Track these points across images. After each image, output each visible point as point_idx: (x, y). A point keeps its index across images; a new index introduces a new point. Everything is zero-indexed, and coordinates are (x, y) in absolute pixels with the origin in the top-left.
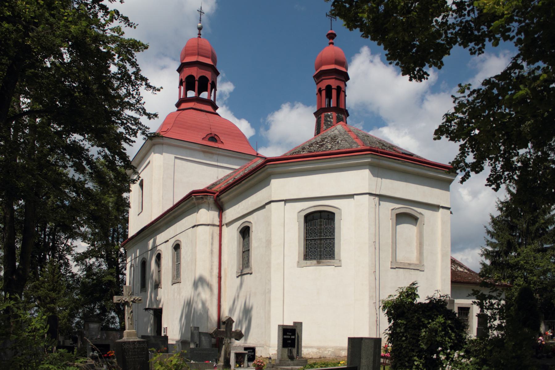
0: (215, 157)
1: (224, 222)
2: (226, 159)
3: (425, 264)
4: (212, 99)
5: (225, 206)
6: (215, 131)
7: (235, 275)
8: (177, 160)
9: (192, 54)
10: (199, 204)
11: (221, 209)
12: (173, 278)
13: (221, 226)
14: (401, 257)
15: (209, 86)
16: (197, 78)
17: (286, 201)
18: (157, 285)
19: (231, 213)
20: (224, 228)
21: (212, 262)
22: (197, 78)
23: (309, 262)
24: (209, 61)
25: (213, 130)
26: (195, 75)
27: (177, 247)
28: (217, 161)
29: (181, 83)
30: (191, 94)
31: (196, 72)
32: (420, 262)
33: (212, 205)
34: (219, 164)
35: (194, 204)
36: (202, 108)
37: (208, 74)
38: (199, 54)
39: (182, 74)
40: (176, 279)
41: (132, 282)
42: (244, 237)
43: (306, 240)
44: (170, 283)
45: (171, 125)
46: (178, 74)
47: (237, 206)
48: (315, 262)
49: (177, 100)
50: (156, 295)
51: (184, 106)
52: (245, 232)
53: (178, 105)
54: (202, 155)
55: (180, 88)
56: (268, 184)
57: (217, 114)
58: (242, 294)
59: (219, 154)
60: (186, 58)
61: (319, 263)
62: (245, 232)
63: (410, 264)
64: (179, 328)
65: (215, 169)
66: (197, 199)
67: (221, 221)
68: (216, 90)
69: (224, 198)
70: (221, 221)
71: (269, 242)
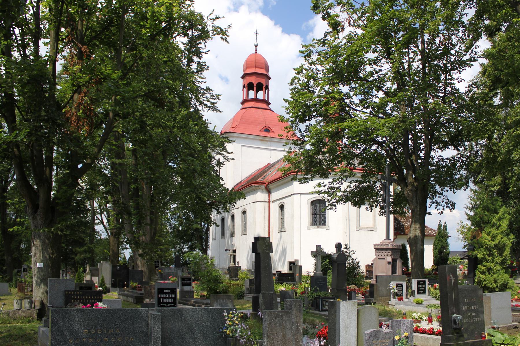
0: (269, 143)
1: (271, 200)
2: (277, 144)
3: (377, 227)
4: (266, 99)
5: (272, 191)
6: (268, 125)
7: (277, 232)
8: (243, 148)
9: (251, 67)
10: (256, 189)
11: (269, 192)
12: (242, 232)
13: (269, 202)
14: (363, 224)
15: (264, 89)
16: (255, 85)
17: (301, 194)
18: (232, 234)
19: (275, 195)
20: (271, 203)
21: (265, 223)
22: (255, 85)
23: (313, 227)
24: (263, 71)
25: (267, 123)
26: (253, 82)
27: (244, 213)
28: (270, 146)
29: (244, 87)
30: (252, 94)
31: (254, 80)
32: (374, 226)
33: (264, 190)
34: (271, 148)
35: (254, 189)
36: (259, 106)
37: (263, 81)
38: (256, 67)
39: (245, 81)
40: (244, 232)
41: (214, 231)
42: (282, 211)
43: (312, 215)
44: (240, 234)
45: (238, 122)
46: (242, 80)
47: (277, 192)
48: (316, 227)
49: (242, 74)
50: (232, 241)
51: (247, 105)
52: (282, 207)
53: (242, 103)
54: (259, 142)
55: (243, 90)
56: (292, 184)
57: (270, 110)
58: (281, 243)
59: (271, 141)
60: (247, 70)
61: (318, 227)
62: (282, 207)
63: (368, 228)
64: (246, 262)
65: (269, 151)
66: (256, 187)
67: (269, 199)
68: (268, 91)
69: (271, 186)
70: (269, 199)
71: (293, 216)
